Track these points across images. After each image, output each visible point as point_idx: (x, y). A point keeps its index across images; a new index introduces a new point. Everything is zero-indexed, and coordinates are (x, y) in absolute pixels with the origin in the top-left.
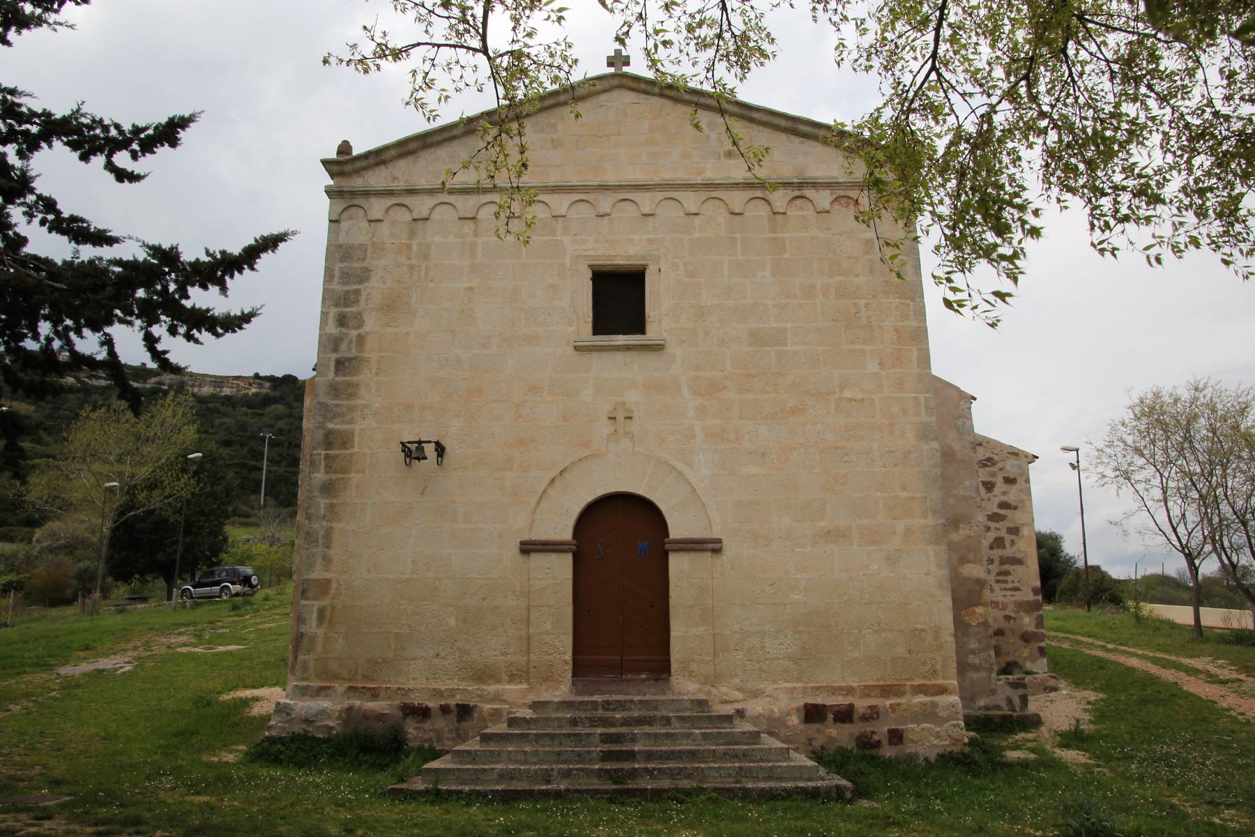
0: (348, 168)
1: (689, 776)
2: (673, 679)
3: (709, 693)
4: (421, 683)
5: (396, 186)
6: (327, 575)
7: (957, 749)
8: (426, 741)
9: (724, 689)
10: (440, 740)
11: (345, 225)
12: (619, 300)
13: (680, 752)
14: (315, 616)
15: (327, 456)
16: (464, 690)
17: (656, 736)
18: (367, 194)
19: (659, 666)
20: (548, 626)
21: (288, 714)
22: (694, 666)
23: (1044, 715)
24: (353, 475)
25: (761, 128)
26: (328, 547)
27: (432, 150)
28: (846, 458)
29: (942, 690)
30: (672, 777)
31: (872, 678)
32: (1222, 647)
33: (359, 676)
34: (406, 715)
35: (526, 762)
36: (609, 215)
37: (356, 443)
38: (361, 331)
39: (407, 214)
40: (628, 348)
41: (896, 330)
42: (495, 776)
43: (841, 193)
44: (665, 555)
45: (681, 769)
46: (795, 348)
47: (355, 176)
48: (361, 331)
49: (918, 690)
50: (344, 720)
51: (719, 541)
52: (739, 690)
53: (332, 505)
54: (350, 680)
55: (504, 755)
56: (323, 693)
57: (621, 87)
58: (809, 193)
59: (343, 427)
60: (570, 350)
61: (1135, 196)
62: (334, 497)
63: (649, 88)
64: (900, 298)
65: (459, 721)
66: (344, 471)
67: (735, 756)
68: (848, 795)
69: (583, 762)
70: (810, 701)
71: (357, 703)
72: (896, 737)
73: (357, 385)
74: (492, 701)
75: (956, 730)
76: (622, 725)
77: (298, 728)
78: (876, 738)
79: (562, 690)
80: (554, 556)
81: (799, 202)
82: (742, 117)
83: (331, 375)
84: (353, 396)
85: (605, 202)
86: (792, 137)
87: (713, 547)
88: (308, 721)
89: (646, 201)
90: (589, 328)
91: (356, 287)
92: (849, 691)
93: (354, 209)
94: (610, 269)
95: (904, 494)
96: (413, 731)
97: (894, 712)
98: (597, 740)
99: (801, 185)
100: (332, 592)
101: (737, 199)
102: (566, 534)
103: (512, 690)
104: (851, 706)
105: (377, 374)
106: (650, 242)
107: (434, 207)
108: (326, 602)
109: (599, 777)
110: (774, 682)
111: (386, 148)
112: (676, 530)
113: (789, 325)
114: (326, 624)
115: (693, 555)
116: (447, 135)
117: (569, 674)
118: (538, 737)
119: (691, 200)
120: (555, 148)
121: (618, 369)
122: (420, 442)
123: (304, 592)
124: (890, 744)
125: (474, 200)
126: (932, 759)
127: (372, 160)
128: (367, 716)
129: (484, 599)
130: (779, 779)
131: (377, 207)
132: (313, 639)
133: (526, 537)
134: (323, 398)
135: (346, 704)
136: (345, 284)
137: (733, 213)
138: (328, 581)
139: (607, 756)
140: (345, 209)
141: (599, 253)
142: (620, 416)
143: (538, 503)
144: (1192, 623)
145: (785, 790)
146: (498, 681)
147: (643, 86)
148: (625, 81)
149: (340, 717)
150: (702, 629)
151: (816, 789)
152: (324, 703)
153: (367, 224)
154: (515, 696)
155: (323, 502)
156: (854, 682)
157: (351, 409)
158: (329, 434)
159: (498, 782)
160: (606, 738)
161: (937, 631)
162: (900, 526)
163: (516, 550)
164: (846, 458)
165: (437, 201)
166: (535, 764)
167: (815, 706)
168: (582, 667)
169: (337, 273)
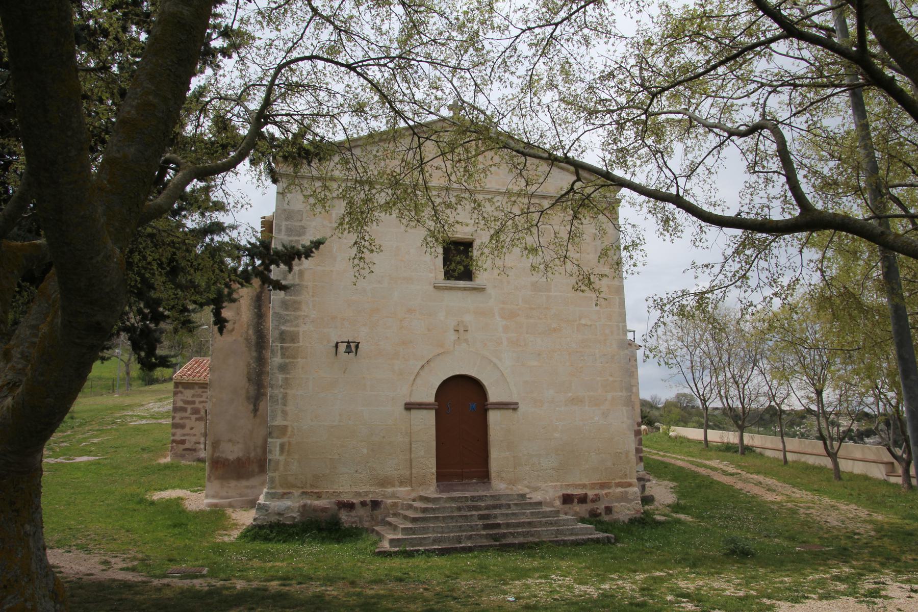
1: (532, 535)
3: (512, 489)
4: (347, 489)
6: (285, 423)
7: (638, 516)
10: (361, 522)
14: (278, 449)
15: (282, 348)
16: (373, 492)
17: (507, 515)
19: (484, 476)
20: (422, 453)
22: (504, 475)
23: (656, 497)
26: (285, 405)
29: (630, 485)
32: (721, 453)
33: (308, 485)
34: (340, 508)
35: (443, 532)
37: (301, 339)
38: (301, 267)
40: (465, 289)
41: (608, 287)
44: (486, 411)
48: (301, 267)
49: (619, 485)
51: (517, 404)
53: (286, 379)
55: (431, 529)
59: (292, 329)
60: (432, 287)
61: (562, 100)
62: (288, 373)
66: (294, 358)
67: (551, 524)
68: (613, 541)
69: (473, 530)
70: (565, 492)
71: (309, 502)
72: (609, 510)
73: (300, 303)
74: (390, 497)
77: (274, 519)
78: (599, 511)
79: (431, 491)
80: (425, 412)
84: (297, 309)
87: (511, 406)
88: (280, 514)
90: (441, 275)
91: (297, 238)
95: (611, 379)
96: (344, 516)
100: (289, 433)
102: (431, 399)
103: (402, 490)
104: (586, 494)
105: (313, 296)
108: (285, 440)
110: (545, 482)
115: (502, 411)
117: (435, 481)
118: (444, 518)
121: (458, 301)
122: (348, 342)
123: (270, 433)
124: (606, 514)
126: (626, 521)
128: (315, 510)
130: (576, 535)
132: (278, 462)
133: (408, 400)
134: (278, 310)
135: (302, 502)
136: (289, 236)
138: (286, 427)
139: (486, 527)
142: (461, 329)
143: (414, 380)
146: (394, 486)
149: (299, 511)
151: (598, 538)
152: (287, 503)
155: (280, 377)
157: (297, 318)
158: (282, 333)
159: (433, 545)
160: (482, 517)
161: (627, 453)
162: (609, 396)
163: (403, 407)
167: (568, 495)
168: (441, 476)
169: (283, 228)
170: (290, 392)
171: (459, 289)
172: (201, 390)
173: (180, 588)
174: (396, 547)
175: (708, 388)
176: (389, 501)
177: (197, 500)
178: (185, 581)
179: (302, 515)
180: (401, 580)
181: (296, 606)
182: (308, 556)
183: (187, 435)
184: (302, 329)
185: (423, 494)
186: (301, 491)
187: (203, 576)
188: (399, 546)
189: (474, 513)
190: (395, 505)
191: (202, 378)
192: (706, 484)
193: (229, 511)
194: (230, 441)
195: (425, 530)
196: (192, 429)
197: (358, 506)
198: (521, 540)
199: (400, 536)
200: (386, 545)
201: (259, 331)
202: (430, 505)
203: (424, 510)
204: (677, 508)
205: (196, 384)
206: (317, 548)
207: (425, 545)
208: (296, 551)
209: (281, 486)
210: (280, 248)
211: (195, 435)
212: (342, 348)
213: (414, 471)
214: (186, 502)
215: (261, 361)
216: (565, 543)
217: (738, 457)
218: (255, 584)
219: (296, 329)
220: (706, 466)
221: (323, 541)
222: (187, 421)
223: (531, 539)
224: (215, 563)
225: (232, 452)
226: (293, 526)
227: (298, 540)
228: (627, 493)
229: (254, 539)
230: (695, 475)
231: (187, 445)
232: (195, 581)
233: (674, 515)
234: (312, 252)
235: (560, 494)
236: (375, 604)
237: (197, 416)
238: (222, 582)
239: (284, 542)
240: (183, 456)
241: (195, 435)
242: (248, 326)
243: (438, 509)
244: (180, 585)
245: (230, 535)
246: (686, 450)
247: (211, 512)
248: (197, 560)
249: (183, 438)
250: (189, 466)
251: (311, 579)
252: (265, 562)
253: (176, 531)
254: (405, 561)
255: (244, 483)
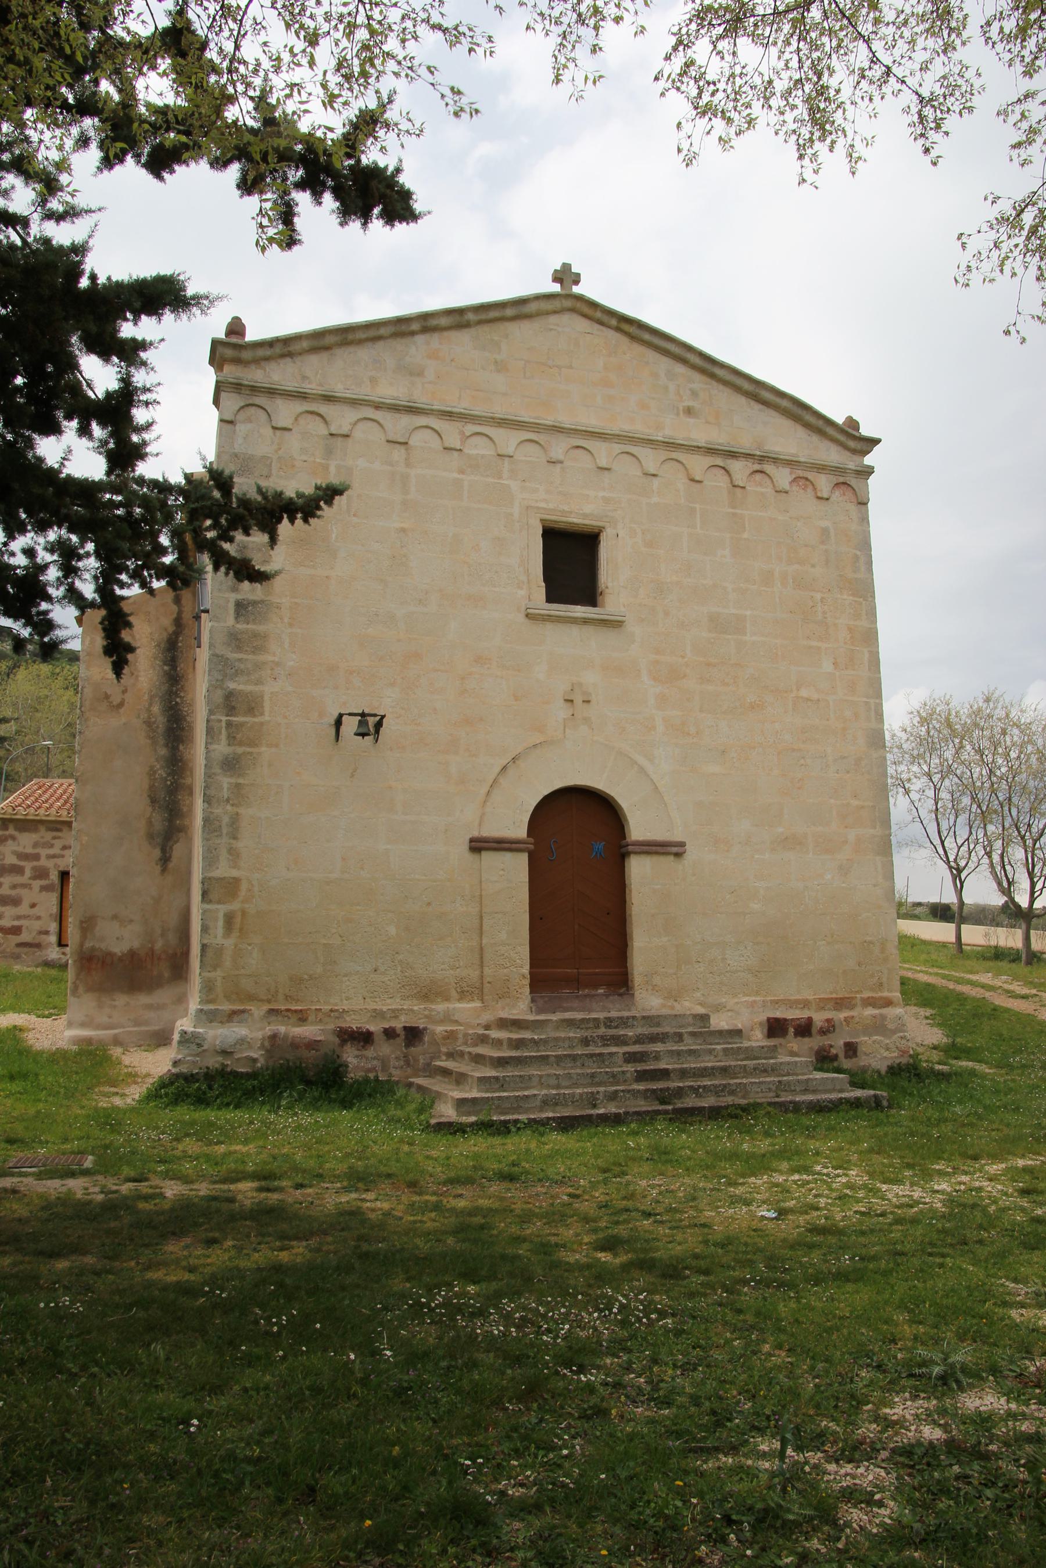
0: (246, 355)
1: (732, 1093)
2: (637, 994)
3: (672, 1008)
5: (311, 387)
6: (235, 873)
7: (904, 1060)
8: (369, 1070)
9: (687, 1004)
10: (385, 1068)
11: (241, 428)
12: (571, 563)
13: (713, 1068)
14: (221, 923)
15: (229, 724)
16: (412, 1012)
17: (679, 1053)
18: (272, 392)
19: (620, 981)
20: (503, 936)
21: (199, 1045)
22: (657, 980)
24: (263, 749)
25: (721, 387)
27: (351, 349)
28: (802, 761)
29: (888, 1003)
30: (717, 1094)
31: (826, 991)
33: (281, 997)
34: (343, 1042)
35: (558, 1087)
36: (561, 462)
39: (322, 425)
40: (586, 621)
41: (850, 629)
42: (538, 1103)
43: (800, 473)
45: (725, 1086)
46: (754, 638)
47: (253, 367)
49: (869, 1002)
50: (267, 1051)
51: (682, 844)
52: (700, 1004)
53: (238, 786)
54: (269, 1001)
55: (535, 1080)
56: (236, 1018)
57: (572, 310)
58: (769, 468)
59: (249, 688)
60: (521, 618)
62: (239, 776)
63: (605, 318)
64: (853, 595)
65: (407, 1046)
66: (252, 744)
68: (885, 1103)
69: (618, 1083)
70: (772, 1015)
71: (282, 1029)
72: (851, 1049)
73: (265, 637)
74: (441, 1022)
75: (904, 1041)
76: (635, 1043)
77: (213, 1062)
78: (834, 1051)
79: (521, 1008)
80: (508, 855)
81: (758, 476)
82: (702, 371)
83: (231, 621)
85: (559, 447)
86: (752, 403)
87: (668, 849)
88: (225, 1053)
89: (604, 453)
92: (806, 1004)
93: (252, 410)
94: (562, 526)
95: (855, 803)
96: (351, 1057)
97: (848, 1025)
98: (619, 1060)
99: (762, 459)
101: (698, 464)
102: (521, 832)
104: (810, 1019)
105: (291, 625)
106: (607, 500)
107: (355, 423)
108: (235, 906)
109: (646, 1098)
110: (735, 995)
111: (297, 338)
112: (638, 829)
113: (748, 613)
114: (236, 934)
115: (655, 859)
116: (372, 333)
117: (527, 990)
118: (559, 1059)
119: (651, 459)
120: (499, 371)
121: (569, 643)
122: (363, 715)
124: (846, 1057)
125: (406, 421)
127: (278, 349)
128: (295, 1044)
129: (429, 904)
131: (285, 412)
135: (269, 1030)
137: (693, 480)
138: (237, 881)
139: (642, 1076)
140: (242, 407)
141: (551, 506)
142: (578, 699)
144: (953, 939)
145: (831, 1101)
146: (447, 999)
147: (598, 314)
148: (579, 305)
150: (665, 939)
151: (857, 1099)
153: (271, 430)
154: (468, 1013)
156: (808, 995)
157: (258, 666)
158: (229, 696)
159: (541, 1110)
160: (631, 1058)
162: (851, 835)
163: (466, 846)
164: (802, 761)
165: (361, 416)
166: (567, 1087)
167: (777, 1020)
170: (245, 812)
171: (574, 621)
172: (49, 836)
173: (41, 1196)
174: (469, 1114)
175: (964, 848)
176: (440, 1029)
177: (52, 1033)
178: (49, 1182)
179: (269, 1053)
180: (511, 1178)
181: (312, 1234)
182: (288, 1132)
183: (25, 917)
184: (268, 689)
185: (504, 1014)
186: (266, 1007)
187: (86, 1173)
188: (475, 1114)
189: (614, 1049)
190: (451, 1036)
191: (53, 811)
192: (983, 1013)
193: (116, 1052)
194: (115, 917)
195: (524, 1081)
196: (33, 906)
197: (379, 1038)
198: (708, 1102)
199: (475, 1094)
200: (447, 1112)
201: (171, 708)
202: (527, 1035)
203: (518, 1044)
204: (952, 1051)
205: (41, 822)
206: (306, 1118)
207: (527, 1111)
208: (267, 1124)
209: (228, 998)
210: (254, 495)
211: (39, 918)
212: (350, 725)
213: (487, 971)
214: (31, 1035)
215: (176, 764)
216: (796, 1107)
217: (1021, 968)
218: (203, 1189)
219: (256, 688)
220: (973, 984)
221: (314, 1105)
222: (23, 892)
223: (729, 1100)
224: (106, 1147)
225: (119, 939)
226: (253, 1075)
227: (263, 1103)
228: (883, 1017)
229: (177, 1099)
230: (962, 999)
231: (25, 937)
232: (71, 1183)
233: (954, 1062)
234: (319, 508)
235: (763, 1017)
236: (482, 1227)
237: (43, 882)
238: (131, 1185)
239: (236, 1107)
240: (17, 957)
241: (39, 918)
242: (152, 697)
243: (545, 1042)
244: (40, 1190)
245: (123, 1095)
246: (924, 956)
247: (80, 1053)
248: (66, 1140)
249: (16, 923)
250: (30, 974)
251: (320, 1176)
252: (210, 1143)
253: (16, 1086)
254: (497, 1140)
255: (143, 999)
